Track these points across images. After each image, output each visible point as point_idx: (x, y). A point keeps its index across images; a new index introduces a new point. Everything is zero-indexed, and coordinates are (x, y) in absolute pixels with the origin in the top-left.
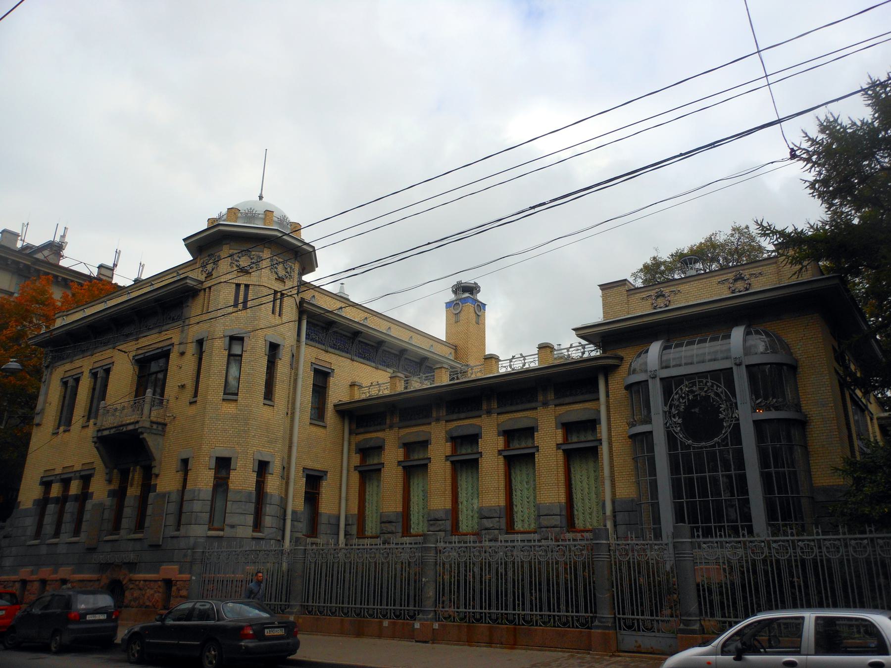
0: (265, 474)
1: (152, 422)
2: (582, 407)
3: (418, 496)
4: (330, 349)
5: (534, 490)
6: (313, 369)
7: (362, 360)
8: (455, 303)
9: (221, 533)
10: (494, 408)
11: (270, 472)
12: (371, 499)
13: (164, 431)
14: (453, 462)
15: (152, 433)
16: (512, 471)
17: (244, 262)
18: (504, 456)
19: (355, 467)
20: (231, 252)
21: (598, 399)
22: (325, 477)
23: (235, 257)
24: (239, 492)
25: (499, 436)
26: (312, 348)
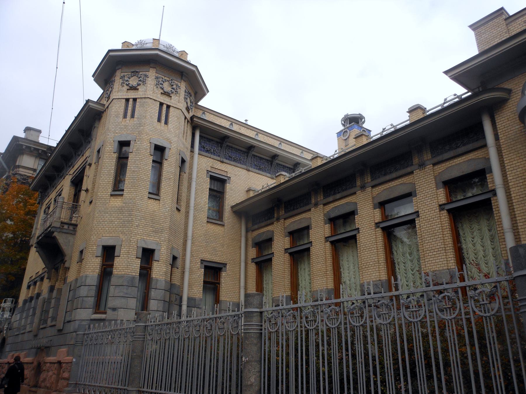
0: (152, 261)
1: (62, 223)
2: (467, 159)
3: (305, 281)
4: (225, 160)
5: (419, 261)
6: (209, 176)
7: (257, 171)
8: (344, 131)
9: (103, 316)
10: (368, 182)
11: (155, 259)
12: (267, 287)
14: (332, 243)
15: (63, 232)
16: (393, 245)
17: (133, 82)
18: (382, 228)
19: (252, 259)
20: (122, 74)
21: (485, 146)
22: (224, 269)
23: (126, 79)
24: (122, 277)
25: (375, 209)
26: (208, 158)
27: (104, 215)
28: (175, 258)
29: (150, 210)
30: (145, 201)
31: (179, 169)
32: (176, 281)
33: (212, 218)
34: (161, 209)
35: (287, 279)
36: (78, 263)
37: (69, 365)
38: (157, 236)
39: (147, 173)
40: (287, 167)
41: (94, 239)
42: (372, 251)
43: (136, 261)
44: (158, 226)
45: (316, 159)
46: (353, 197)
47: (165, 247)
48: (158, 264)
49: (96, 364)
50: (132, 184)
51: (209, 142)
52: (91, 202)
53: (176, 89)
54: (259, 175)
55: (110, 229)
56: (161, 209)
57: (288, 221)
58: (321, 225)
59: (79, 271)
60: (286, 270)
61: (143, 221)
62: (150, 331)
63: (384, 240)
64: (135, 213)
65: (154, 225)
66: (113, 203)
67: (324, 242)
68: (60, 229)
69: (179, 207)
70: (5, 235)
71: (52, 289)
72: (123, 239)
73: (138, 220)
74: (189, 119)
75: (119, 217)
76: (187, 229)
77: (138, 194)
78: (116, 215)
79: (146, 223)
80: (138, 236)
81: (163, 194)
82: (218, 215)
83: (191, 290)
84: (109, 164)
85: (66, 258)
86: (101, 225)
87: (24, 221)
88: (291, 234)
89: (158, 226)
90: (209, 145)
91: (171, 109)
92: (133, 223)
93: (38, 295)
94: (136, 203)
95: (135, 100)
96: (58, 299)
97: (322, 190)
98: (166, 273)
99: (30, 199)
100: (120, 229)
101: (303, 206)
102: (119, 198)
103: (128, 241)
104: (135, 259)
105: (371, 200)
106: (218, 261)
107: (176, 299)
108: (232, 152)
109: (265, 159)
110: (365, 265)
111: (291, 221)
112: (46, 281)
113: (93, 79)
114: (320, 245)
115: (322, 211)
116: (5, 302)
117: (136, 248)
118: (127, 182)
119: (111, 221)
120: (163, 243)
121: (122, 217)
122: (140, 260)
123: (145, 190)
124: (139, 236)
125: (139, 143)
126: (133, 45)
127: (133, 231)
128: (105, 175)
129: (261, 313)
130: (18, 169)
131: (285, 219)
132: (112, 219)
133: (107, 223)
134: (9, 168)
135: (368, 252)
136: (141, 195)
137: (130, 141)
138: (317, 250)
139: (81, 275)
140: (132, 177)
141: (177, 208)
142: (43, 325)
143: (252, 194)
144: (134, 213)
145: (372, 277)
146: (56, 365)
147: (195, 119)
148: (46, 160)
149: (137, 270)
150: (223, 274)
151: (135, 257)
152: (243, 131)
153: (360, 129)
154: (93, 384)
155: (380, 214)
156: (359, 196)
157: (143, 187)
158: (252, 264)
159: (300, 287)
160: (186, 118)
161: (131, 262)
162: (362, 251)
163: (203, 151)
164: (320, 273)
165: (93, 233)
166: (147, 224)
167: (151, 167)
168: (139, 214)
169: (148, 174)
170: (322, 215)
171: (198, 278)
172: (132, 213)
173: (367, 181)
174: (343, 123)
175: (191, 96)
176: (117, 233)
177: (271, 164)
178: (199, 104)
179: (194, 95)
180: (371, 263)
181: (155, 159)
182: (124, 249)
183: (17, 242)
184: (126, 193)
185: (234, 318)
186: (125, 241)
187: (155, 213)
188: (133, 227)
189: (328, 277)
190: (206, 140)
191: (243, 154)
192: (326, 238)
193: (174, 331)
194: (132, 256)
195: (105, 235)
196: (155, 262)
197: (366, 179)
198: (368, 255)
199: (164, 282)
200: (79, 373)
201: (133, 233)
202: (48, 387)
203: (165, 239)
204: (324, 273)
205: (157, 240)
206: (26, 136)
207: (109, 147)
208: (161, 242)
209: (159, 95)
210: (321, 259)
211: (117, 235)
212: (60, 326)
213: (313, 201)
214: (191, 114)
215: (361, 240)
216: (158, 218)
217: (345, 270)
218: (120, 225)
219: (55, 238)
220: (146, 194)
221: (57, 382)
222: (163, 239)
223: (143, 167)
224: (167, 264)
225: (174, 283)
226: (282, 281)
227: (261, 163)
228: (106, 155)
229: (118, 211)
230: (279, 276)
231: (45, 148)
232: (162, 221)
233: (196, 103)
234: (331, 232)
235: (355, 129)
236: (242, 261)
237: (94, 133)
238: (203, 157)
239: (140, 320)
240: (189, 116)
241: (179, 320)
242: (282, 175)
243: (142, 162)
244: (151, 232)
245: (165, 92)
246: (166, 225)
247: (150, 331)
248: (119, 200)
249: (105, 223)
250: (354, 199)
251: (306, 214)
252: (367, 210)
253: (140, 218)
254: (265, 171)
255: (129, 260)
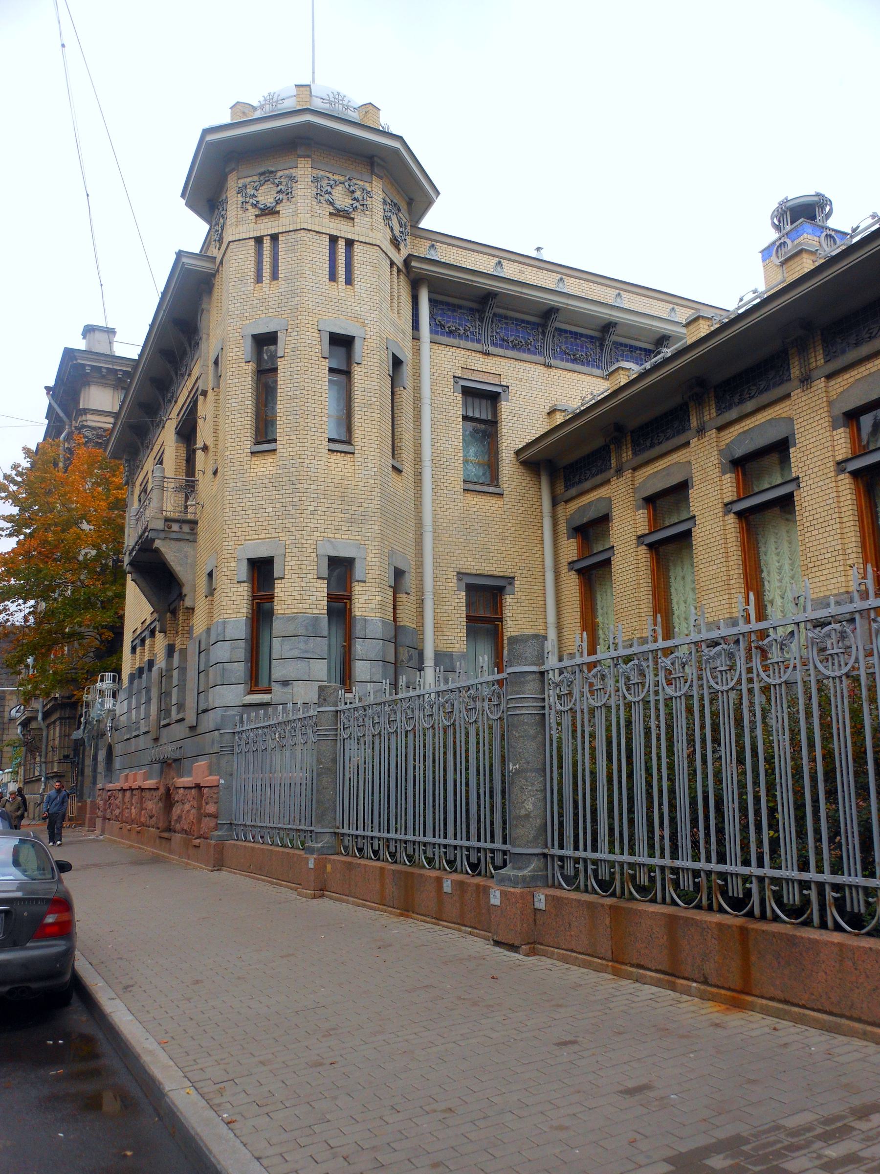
0: (351, 583)
1: (167, 520)
3: (685, 603)
4: (492, 349)
7: (570, 365)
8: (778, 244)
13: (193, 532)
14: (740, 514)
15: (171, 539)
19: (569, 563)
20: (241, 182)
22: (508, 588)
23: (250, 191)
24: (292, 618)
25: (834, 429)
26: (453, 350)
27: (244, 496)
28: (399, 574)
29: (336, 477)
30: (323, 459)
31: (389, 381)
32: (407, 619)
33: (476, 480)
34: (359, 471)
35: (645, 601)
36: (206, 597)
37: (215, 790)
38: (357, 529)
39: (320, 398)
40: (641, 349)
41: (230, 547)
42: (830, 528)
43: (318, 585)
44: (356, 508)
45: (697, 324)
46: (783, 405)
47: (376, 551)
48: (364, 588)
49: (259, 788)
50: (291, 425)
51: (453, 311)
52: (215, 473)
53: (363, 200)
54: (575, 375)
55: (258, 524)
56: (359, 471)
57: (641, 472)
58: (714, 476)
59: (210, 614)
60: (642, 581)
61: (323, 501)
62: (346, 721)
63: (858, 499)
64: (306, 486)
65: (347, 507)
66: (258, 470)
67: (721, 514)
68: (166, 533)
69: (396, 465)
70: (83, 552)
71: (170, 650)
72: (288, 542)
73: (312, 500)
74: (401, 266)
75: (273, 497)
76: (421, 509)
77: (306, 445)
78: (267, 493)
79: (329, 505)
80: (316, 534)
81: (359, 440)
82: (488, 473)
83: (441, 637)
84: (240, 388)
85: (185, 590)
86: (240, 517)
87: (109, 521)
88: (651, 501)
89: (356, 508)
90: (454, 318)
91: (356, 246)
92: (303, 507)
93: (151, 663)
94: (305, 465)
95: (275, 238)
96: (183, 670)
97: (712, 394)
98: (383, 606)
99: (114, 476)
100: (278, 522)
101: (674, 436)
102: (269, 457)
103: (297, 545)
104: (315, 580)
105: (826, 409)
106: (496, 573)
107: (410, 658)
108: (506, 329)
109: (587, 336)
110: (813, 559)
111: (647, 474)
112: (159, 636)
113: (183, 202)
114: (712, 522)
115: (715, 444)
116: (102, 681)
117: (315, 559)
118: (282, 422)
119: (257, 507)
120: (369, 543)
121: (280, 496)
122: (326, 581)
123: (319, 434)
124: (319, 534)
125: (295, 334)
126: (254, 109)
127: (305, 524)
128: (234, 412)
129: (542, 673)
130: (84, 418)
131: (634, 469)
132: (261, 502)
133: (250, 512)
134: (68, 415)
135: (821, 531)
136: (313, 445)
137: (276, 332)
138: (707, 532)
139: (215, 620)
140: (289, 409)
141: (393, 467)
142: (164, 719)
143: (559, 419)
144: (302, 486)
145: (830, 587)
146: (193, 791)
147: (413, 264)
148: (126, 389)
149: (322, 603)
150: (508, 600)
151: (315, 576)
152: (531, 276)
153: (818, 233)
154: (259, 824)
155: (849, 441)
156: (797, 402)
157: (316, 430)
158: (570, 573)
159: (675, 617)
160: (392, 264)
161: (308, 589)
162: (806, 530)
163: (442, 334)
164: (716, 585)
165: (226, 535)
166: (333, 506)
167: (327, 384)
168: (313, 487)
169: (323, 399)
170: (716, 453)
171: (454, 611)
172: (298, 486)
173: (814, 364)
174: (777, 223)
175: (399, 210)
176: (273, 531)
177: (602, 346)
178: (422, 225)
179: (405, 207)
180: (829, 555)
181: (334, 366)
182: (291, 563)
183: (106, 564)
184: (281, 447)
185: (493, 688)
186: (291, 546)
187: (347, 482)
188: (304, 516)
189: (733, 591)
190: (445, 307)
191: (533, 329)
192: (726, 505)
193: (387, 717)
194: (308, 576)
195: (249, 537)
196: (356, 584)
197: (813, 360)
198: (820, 536)
199: (380, 624)
200: (234, 805)
201: (305, 529)
202: (186, 831)
203: (374, 535)
204: (722, 583)
205: (357, 538)
206: (88, 344)
207: (235, 350)
208: (367, 543)
209: (326, 220)
210: (717, 552)
211: (274, 535)
212: (191, 719)
213: (694, 423)
214: (404, 253)
215: (804, 505)
216: (353, 491)
217: (772, 575)
218: (278, 514)
219: (157, 551)
220: (323, 443)
221: (199, 821)
222: (370, 535)
223: (310, 385)
224: (382, 586)
225: (402, 624)
226: (634, 607)
227: (577, 345)
228: (232, 370)
229: (270, 485)
230: (627, 597)
231: (127, 365)
232: (363, 497)
233: (415, 226)
234: (738, 493)
235: (805, 235)
236: (547, 569)
237: (202, 325)
238: (442, 347)
239: (325, 700)
240: (399, 260)
241: (394, 697)
242: (622, 368)
243: (306, 376)
244: (343, 524)
245: (339, 211)
246: (373, 506)
247: (346, 721)
248: (269, 461)
249: (248, 512)
250: (785, 409)
251: (680, 453)
252: (817, 433)
253: (315, 496)
254: (588, 364)
255: (304, 584)
